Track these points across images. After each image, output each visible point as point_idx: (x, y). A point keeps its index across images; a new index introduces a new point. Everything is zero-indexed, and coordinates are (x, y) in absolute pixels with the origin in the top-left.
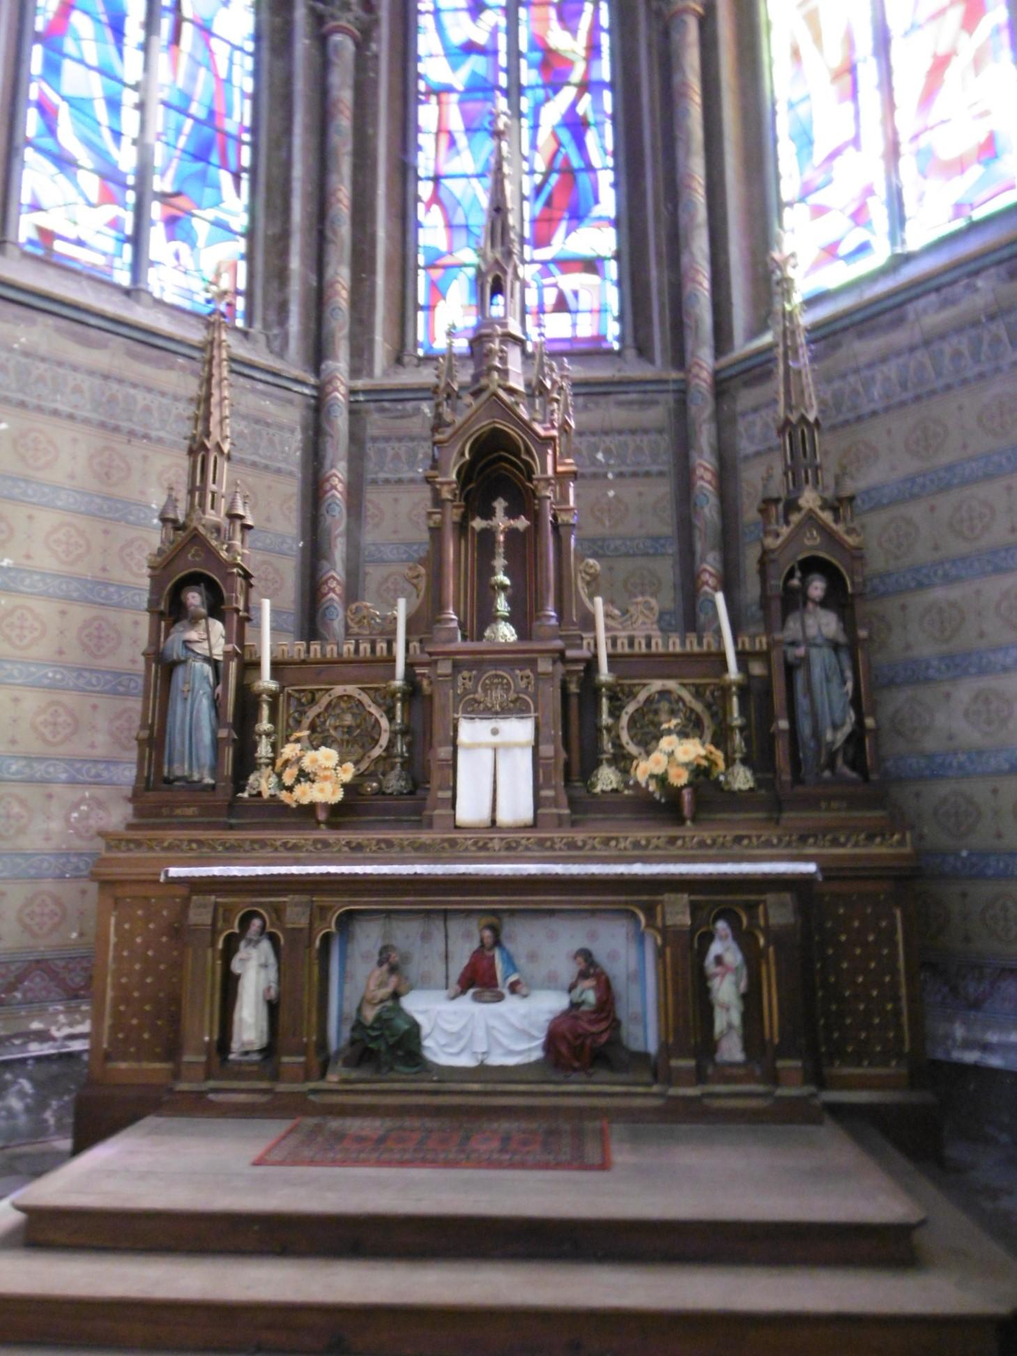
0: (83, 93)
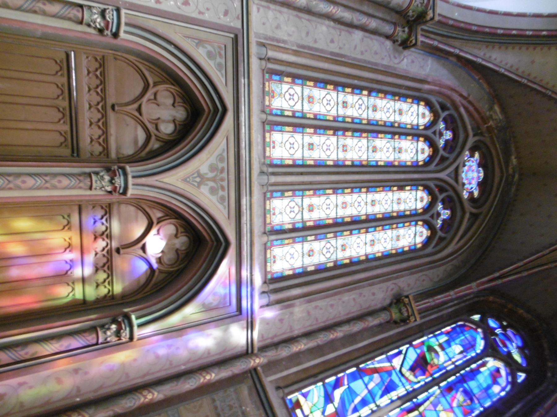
0: (358, 393)
